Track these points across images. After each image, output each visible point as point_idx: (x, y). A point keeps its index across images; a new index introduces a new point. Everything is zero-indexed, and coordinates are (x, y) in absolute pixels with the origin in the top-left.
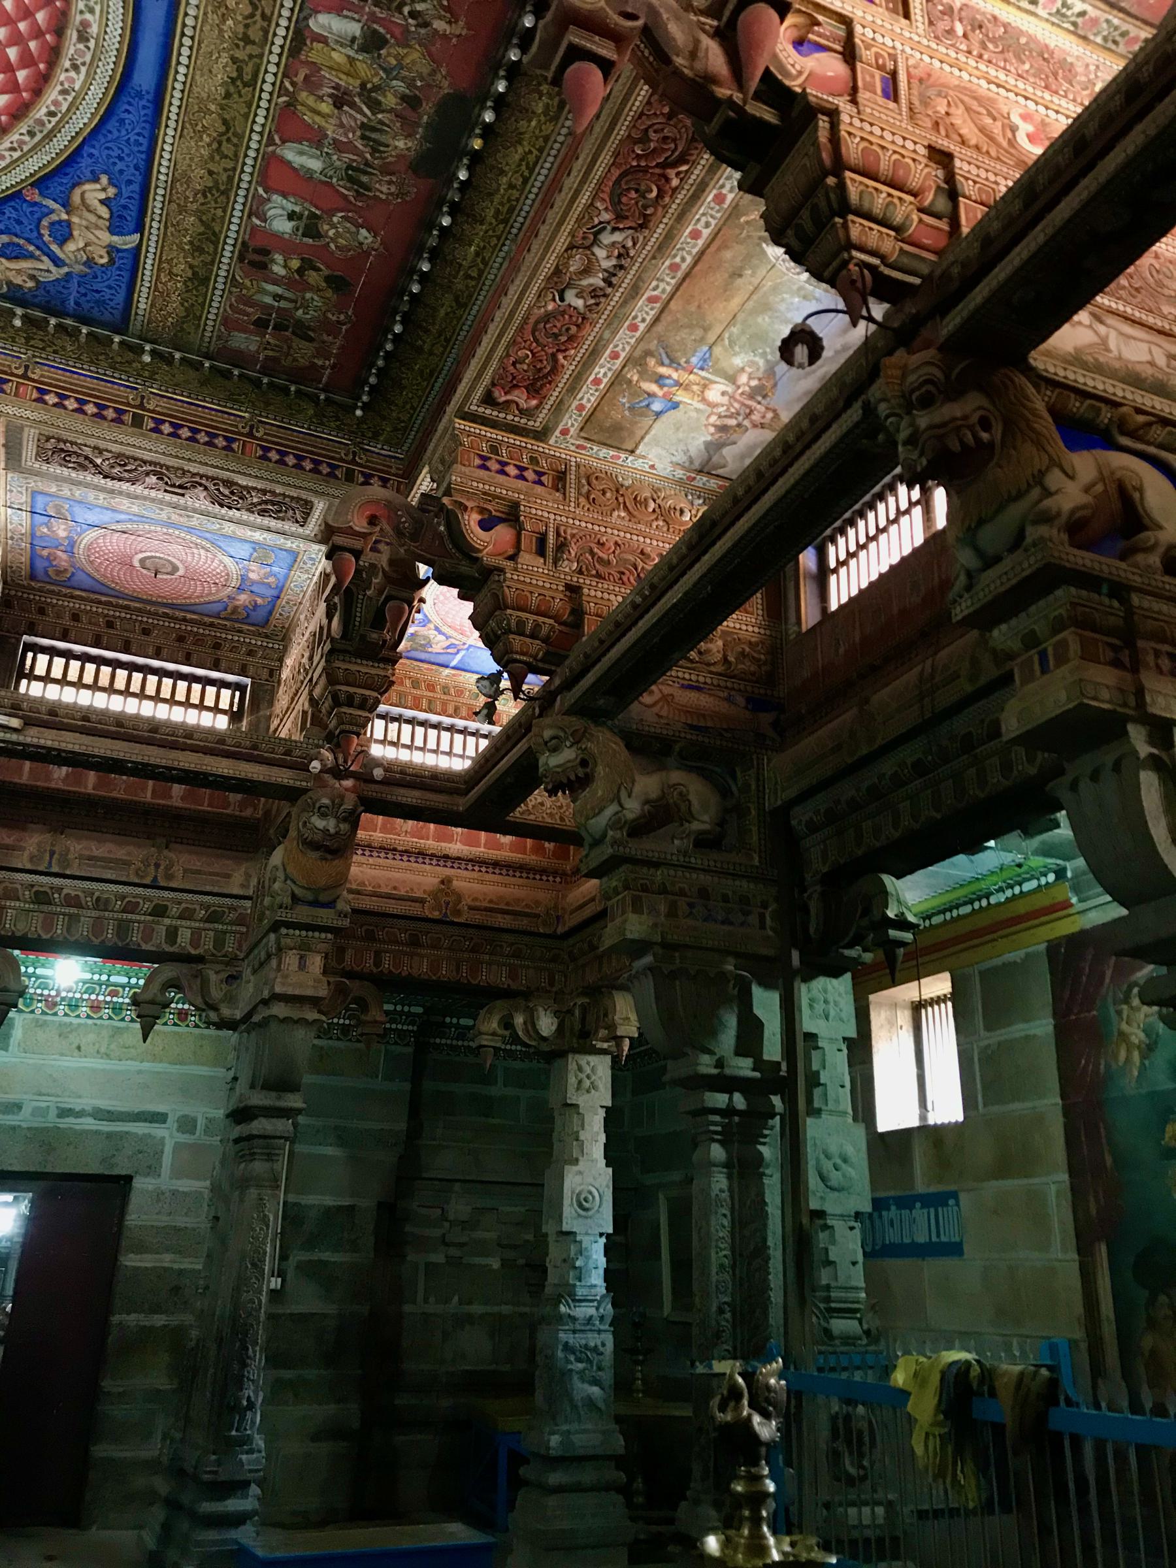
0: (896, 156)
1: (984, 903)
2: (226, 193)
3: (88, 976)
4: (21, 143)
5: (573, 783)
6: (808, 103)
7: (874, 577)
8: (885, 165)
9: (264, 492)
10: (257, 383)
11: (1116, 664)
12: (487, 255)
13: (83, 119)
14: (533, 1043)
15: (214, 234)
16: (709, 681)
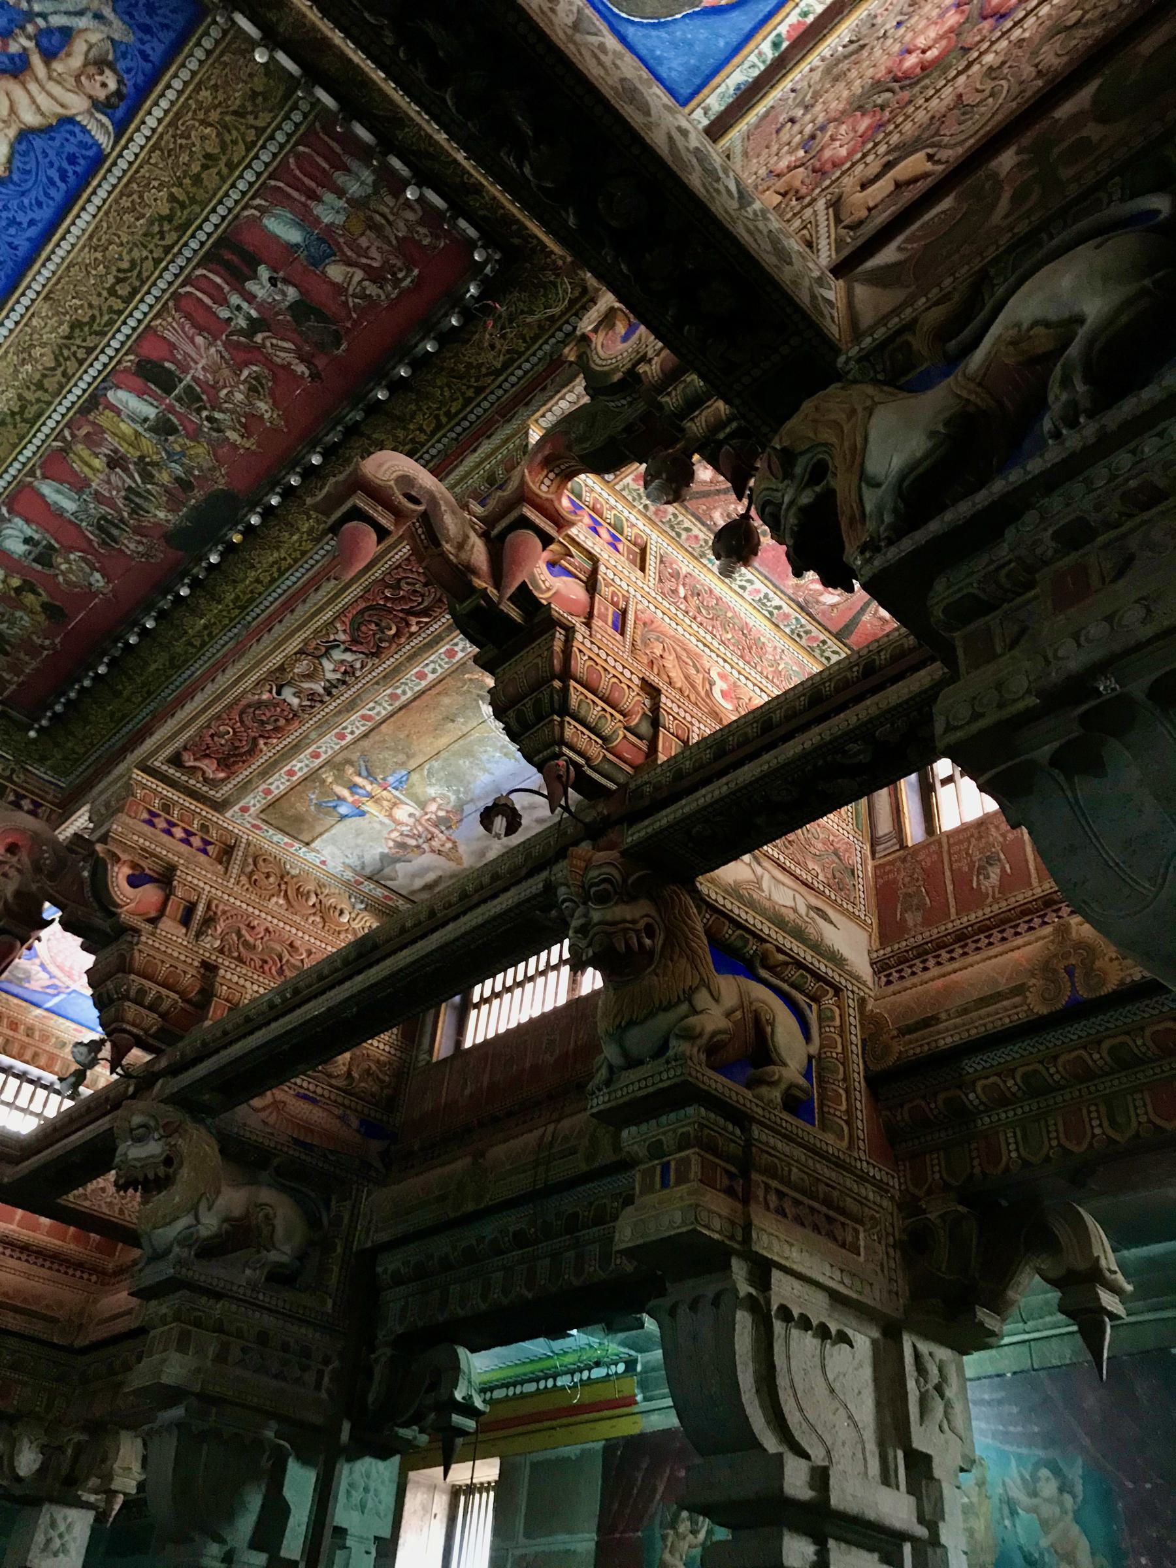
1: (550, 1383)
5: (150, 1182)
6: (550, 615)
7: (513, 1025)
8: (605, 683)
11: (730, 1191)
16: (326, 1094)
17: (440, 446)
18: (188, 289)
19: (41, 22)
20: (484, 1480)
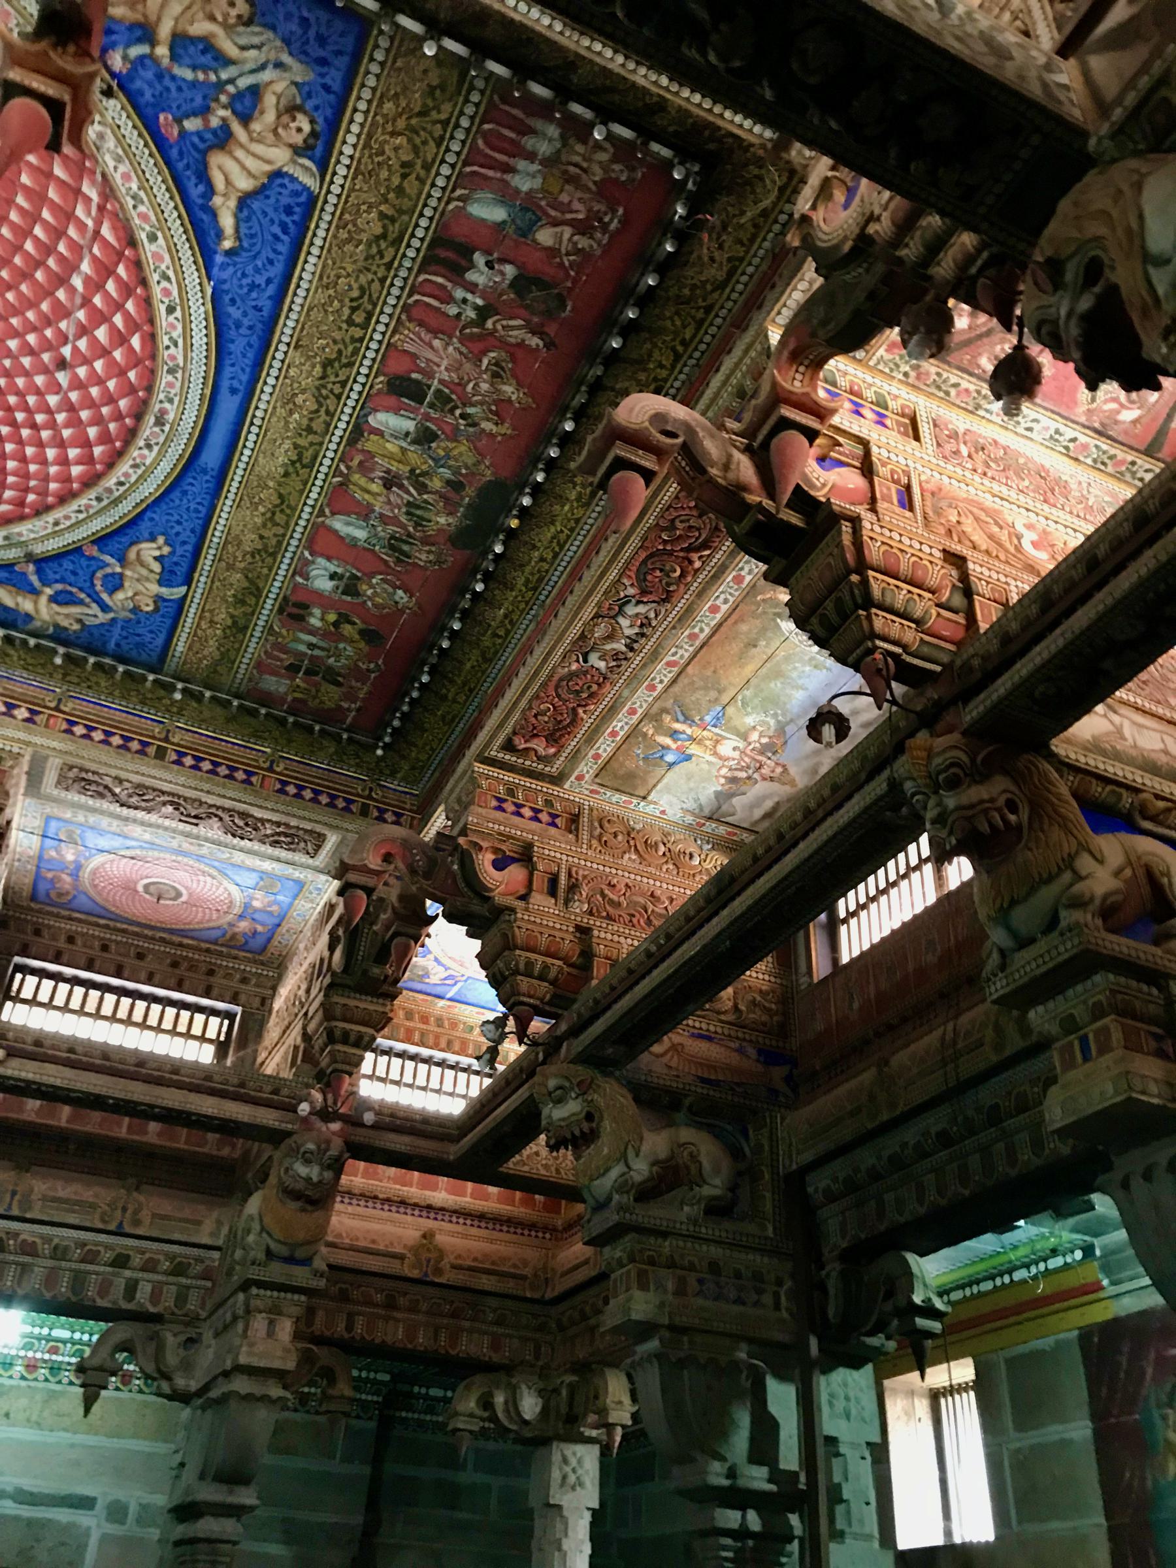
0: (914, 559)
1: (1007, 1279)
2: (273, 555)
3: (29, 1329)
4: (88, 507)
5: (577, 1139)
7: (886, 932)
8: (904, 567)
9: (278, 824)
10: (282, 722)
12: (515, 617)
13: (150, 489)
14: (514, 1427)
15: (258, 589)
16: (719, 1030)
17: (682, 377)
18: (416, 297)
19: (231, 89)
20: (961, 1381)
